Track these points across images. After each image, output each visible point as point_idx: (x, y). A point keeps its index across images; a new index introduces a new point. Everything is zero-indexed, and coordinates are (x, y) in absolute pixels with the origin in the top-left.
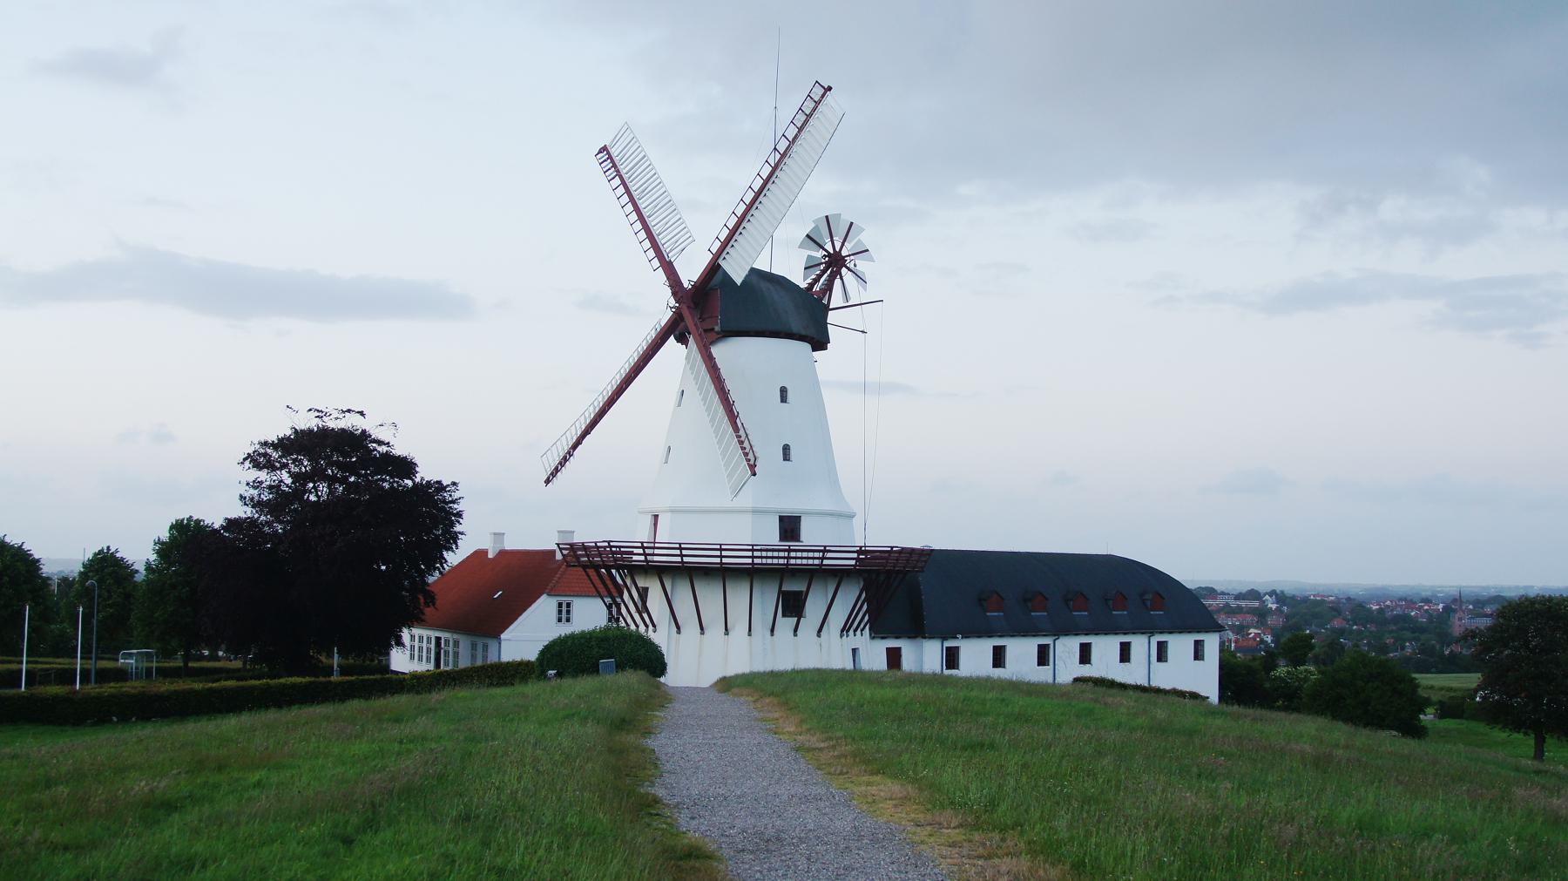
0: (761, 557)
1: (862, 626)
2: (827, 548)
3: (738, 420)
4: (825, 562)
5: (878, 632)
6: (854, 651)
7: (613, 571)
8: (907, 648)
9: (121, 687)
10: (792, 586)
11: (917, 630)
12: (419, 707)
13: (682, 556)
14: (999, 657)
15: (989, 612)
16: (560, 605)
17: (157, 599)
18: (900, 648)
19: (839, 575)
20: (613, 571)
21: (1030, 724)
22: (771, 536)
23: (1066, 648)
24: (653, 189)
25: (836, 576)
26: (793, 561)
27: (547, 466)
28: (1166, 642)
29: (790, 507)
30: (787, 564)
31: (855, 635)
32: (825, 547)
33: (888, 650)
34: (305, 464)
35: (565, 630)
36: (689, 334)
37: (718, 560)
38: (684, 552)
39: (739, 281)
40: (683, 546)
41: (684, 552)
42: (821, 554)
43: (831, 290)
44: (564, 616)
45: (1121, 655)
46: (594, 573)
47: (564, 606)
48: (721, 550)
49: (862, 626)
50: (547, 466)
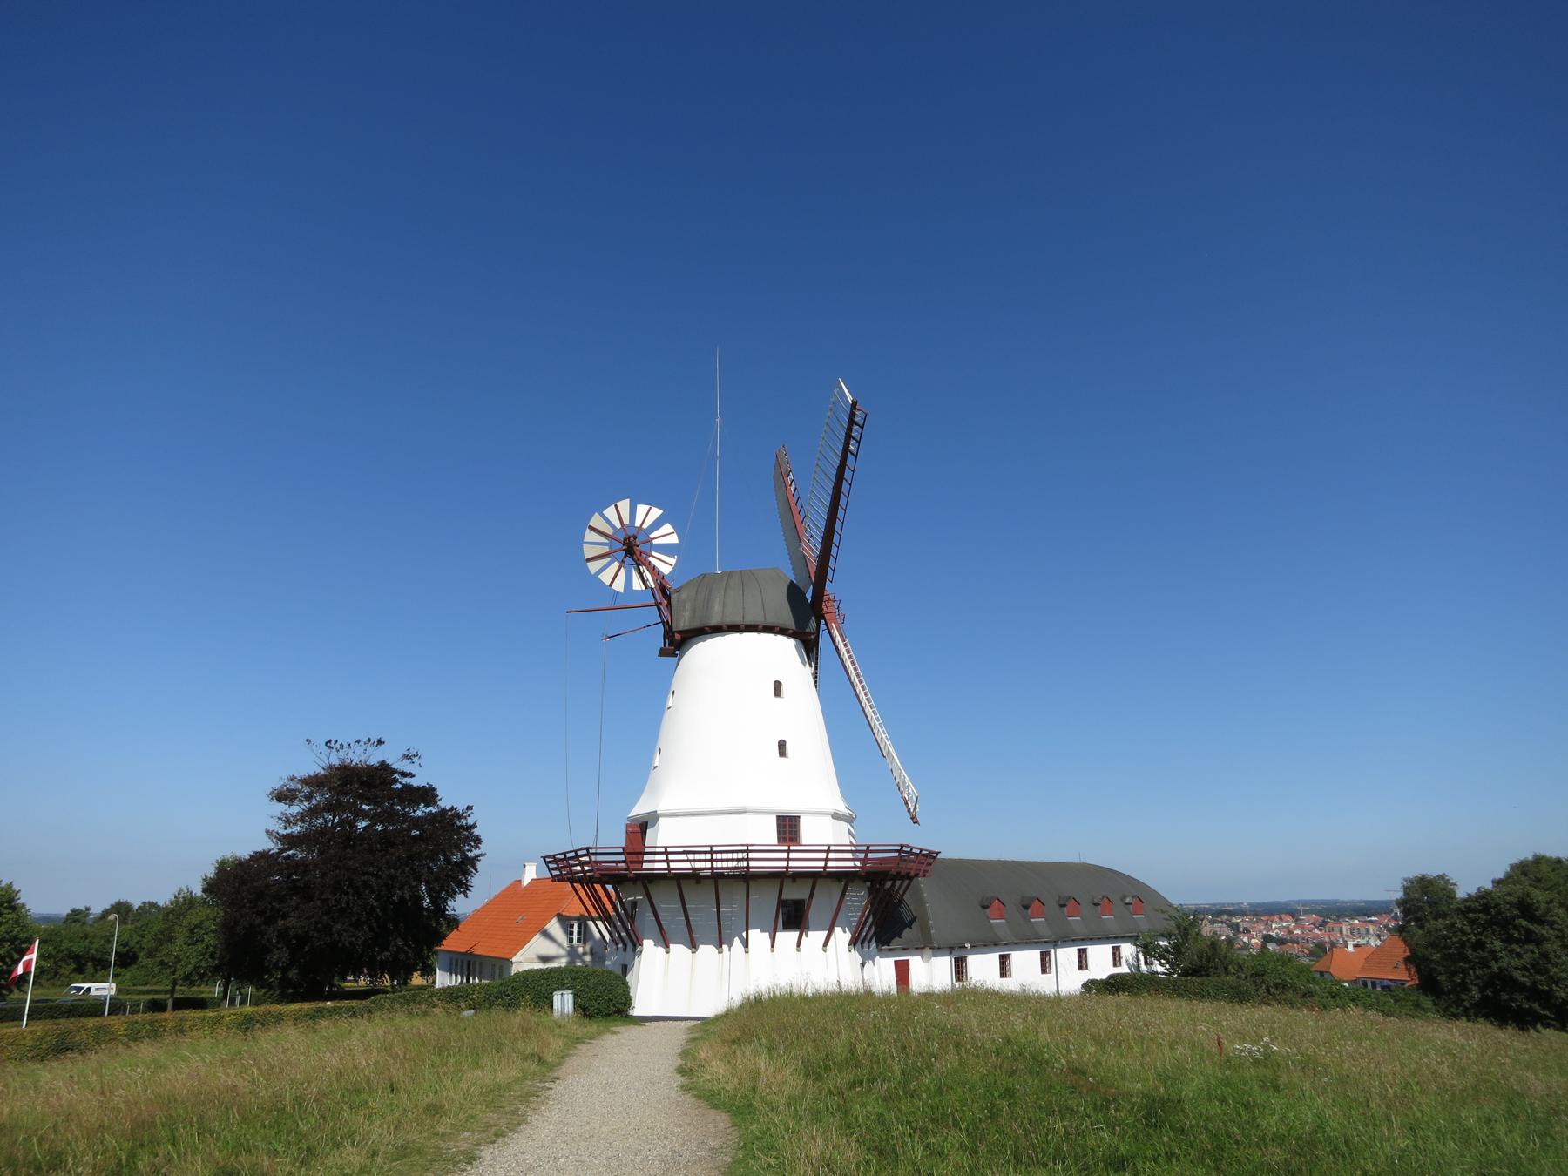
0: (722, 860)
1: (869, 938)
2: (871, 848)
4: (830, 864)
8: (916, 963)
10: (794, 893)
11: (928, 945)
12: (102, 1142)
13: (667, 861)
16: (451, 960)
19: (844, 878)
21: (1158, 1099)
22: (766, 833)
23: (1066, 956)
25: (840, 881)
26: (719, 864)
28: (908, 960)
29: (789, 807)
31: (862, 947)
32: (868, 847)
35: (1086, 976)
38: (671, 857)
40: (669, 850)
41: (671, 857)
44: (1118, 964)
45: (1114, 959)
46: (580, 886)
47: (497, 967)
48: (711, 852)
49: (869, 938)
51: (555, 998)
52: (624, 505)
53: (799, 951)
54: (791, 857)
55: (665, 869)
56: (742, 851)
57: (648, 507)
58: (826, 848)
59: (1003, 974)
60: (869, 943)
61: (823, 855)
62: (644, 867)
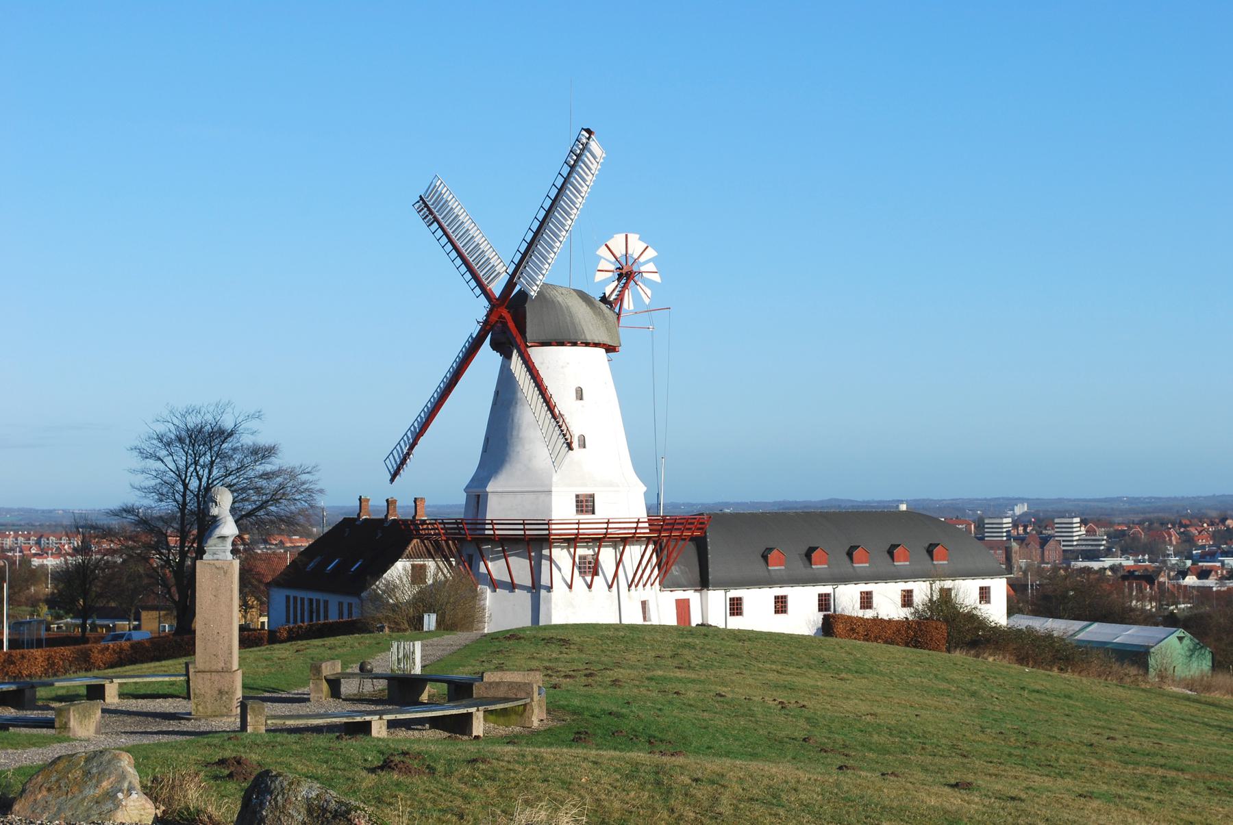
5: (667, 583)
6: (644, 604)
7: (450, 542)
14: (736, 607)
16: (288, 598)
17: (583, 780)
18: (688, 600)
20: (450, 542)
24: (472, 250)
27: (390, 467)
30: (525, 535)
33: (678, 601)
36: (513, 346)
37: (522, 532)
39: (597, 253)
43: (622, 300)
50: (390, 467)
51: (425, 616)
53: (644, 590)
54: (605, 530)
55: (522, 535)
56: (577, 523)
57: (510, 274)
58: (607, 521)
59: (644, 604)
60: (652, 585)
61: (605, 526)
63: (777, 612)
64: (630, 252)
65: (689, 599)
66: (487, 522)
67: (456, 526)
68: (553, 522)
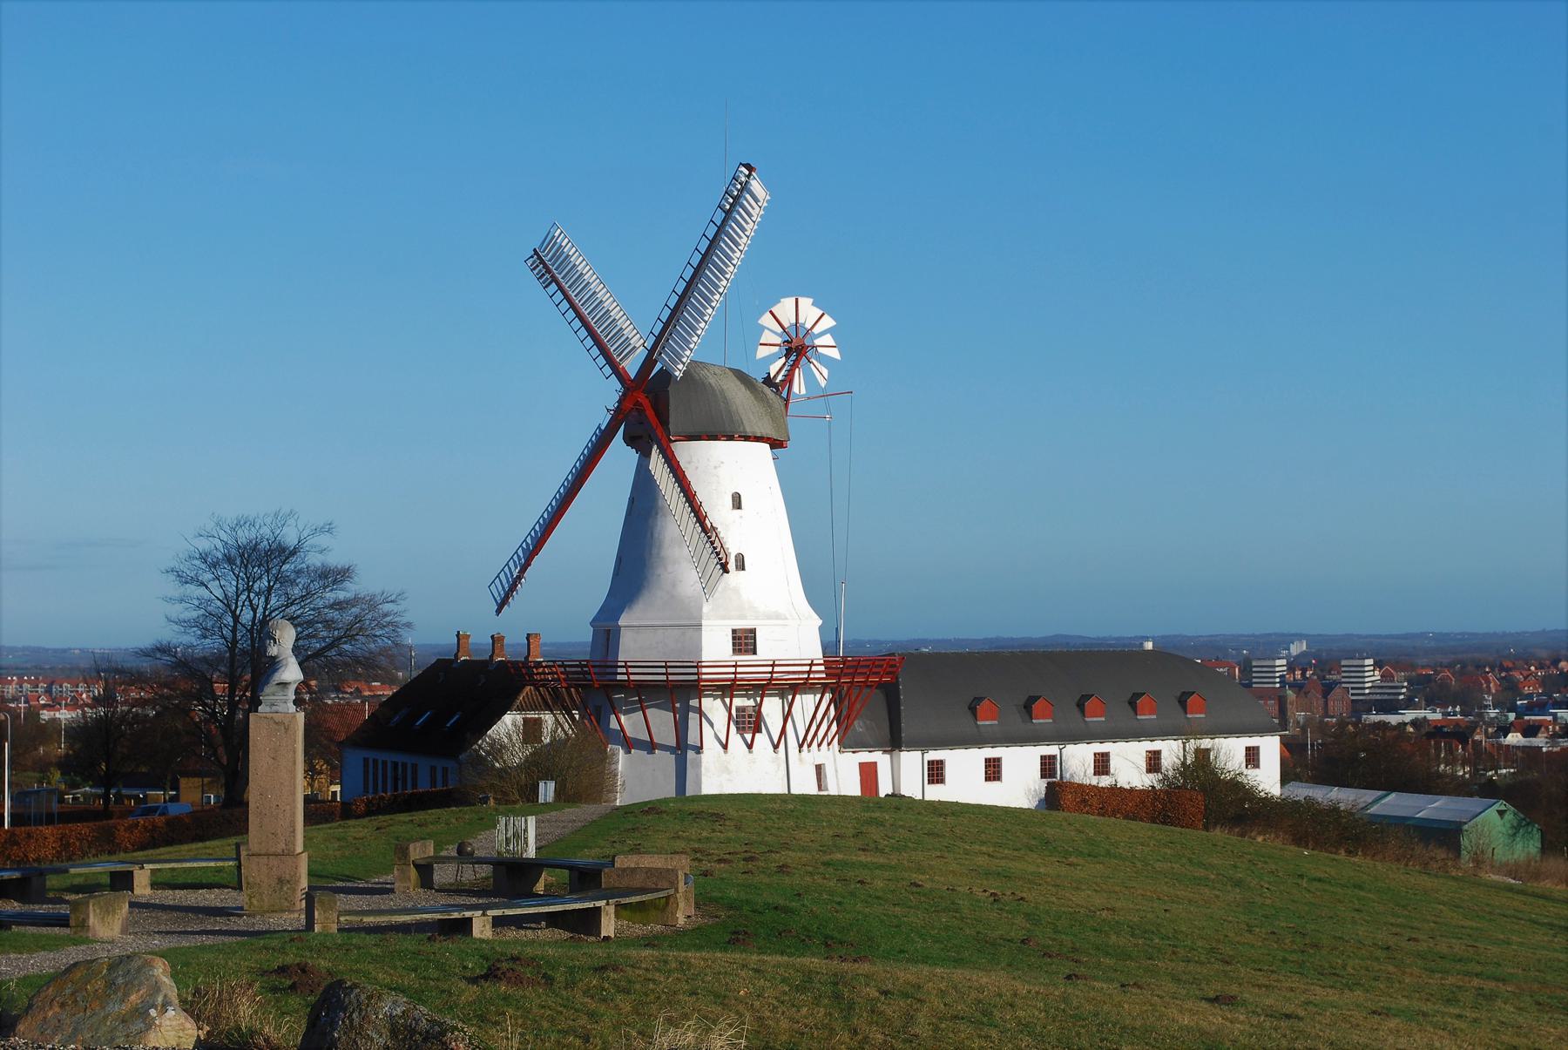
2: (776, 663)
3: (707, 521)
6: (819, 769)
9: (60, 908)
11: (894, 743)
14: (936, 773)
15: (417, 721)
27: (496, 595)
30: (667, 680)
34: (247, 694)
37: (664, 678)
42: (775, 670)
50: (496, 595)
51: (540, 784)
52: (827, 322)
54: (775, 670)
56: (733, 666)
58: (771, 663)
60: (829, 744)
61: (770, 669)
62: (1285, 660)
63: (988, 779)
64: (801, 320)
65: (876, 763)
66: (619, 664)
67: (580, 669)
68: (703, 664)
